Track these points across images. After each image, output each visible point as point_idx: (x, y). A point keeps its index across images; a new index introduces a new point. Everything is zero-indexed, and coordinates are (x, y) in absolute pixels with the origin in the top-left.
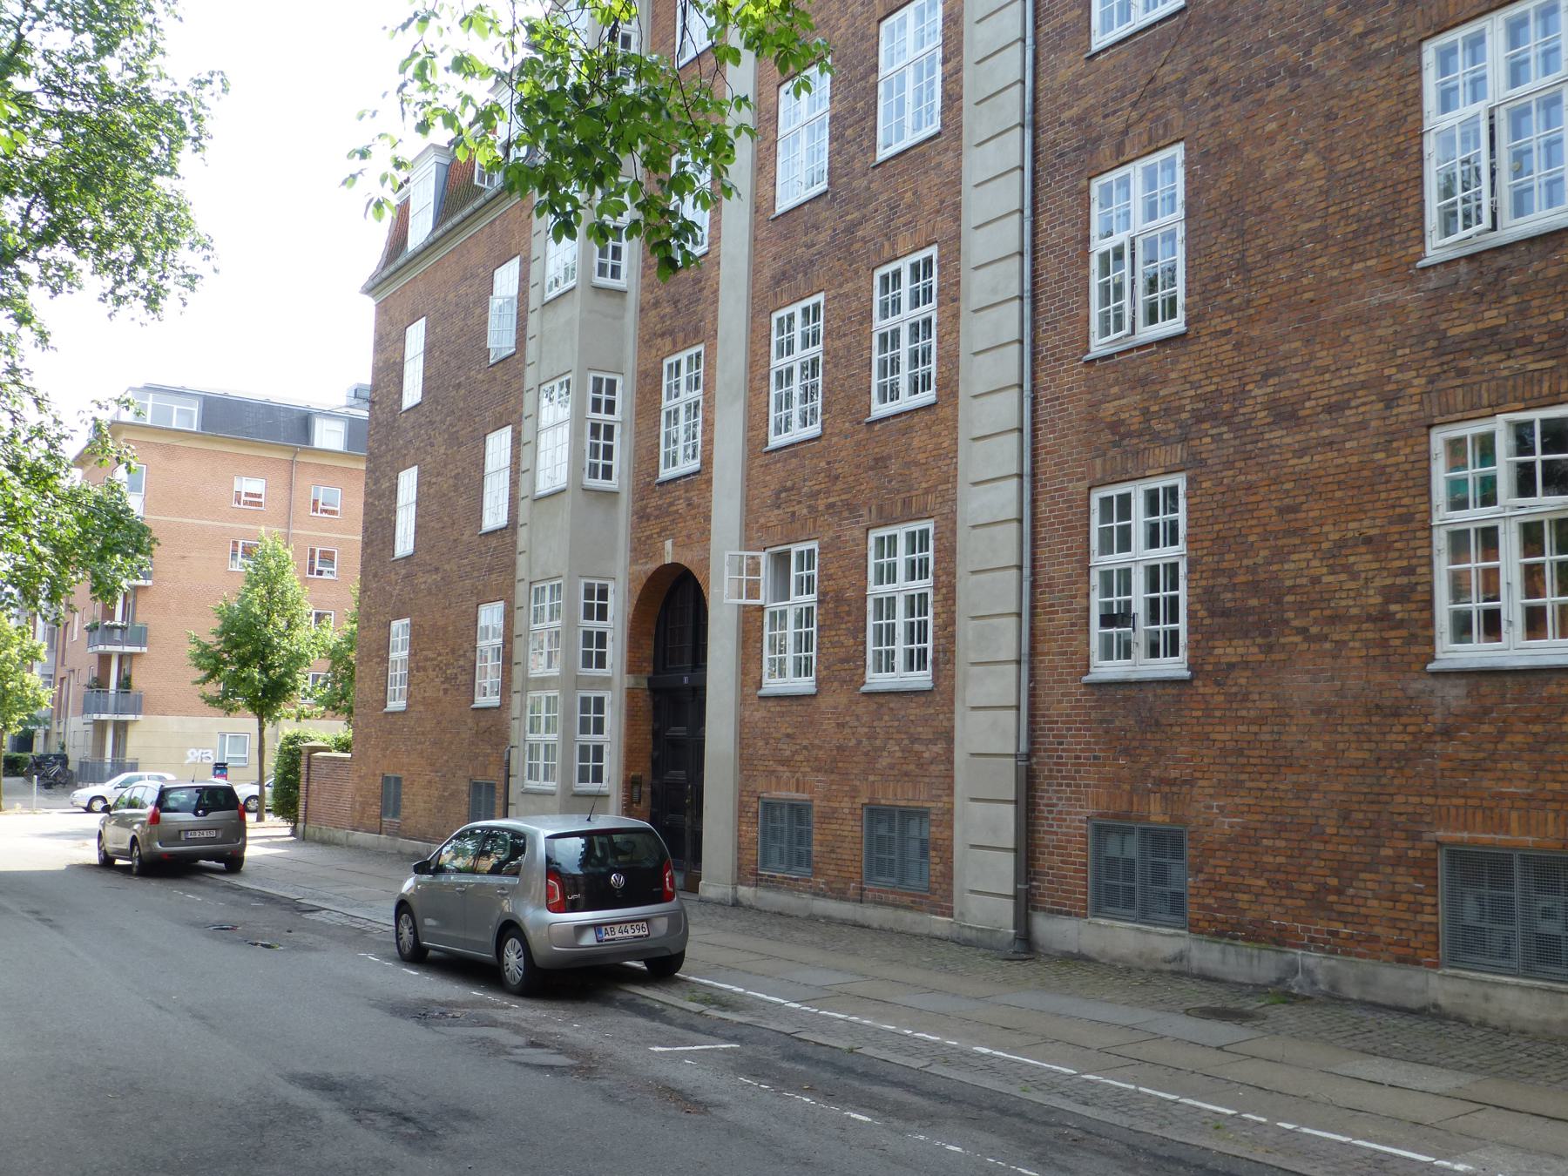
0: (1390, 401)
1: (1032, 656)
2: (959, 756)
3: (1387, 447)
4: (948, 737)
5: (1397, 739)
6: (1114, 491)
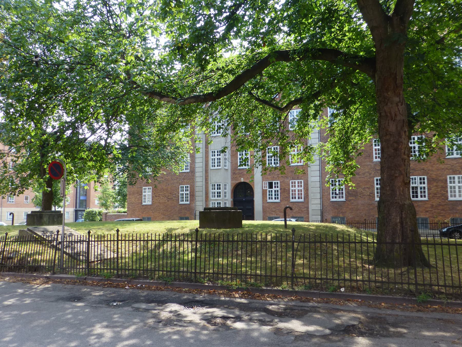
0: (370, 174)
1: (322, 198)
2: (310, 210)
3: (370, 178)
4: (308, 208)
5: (371, 207)
6: (182, 186)
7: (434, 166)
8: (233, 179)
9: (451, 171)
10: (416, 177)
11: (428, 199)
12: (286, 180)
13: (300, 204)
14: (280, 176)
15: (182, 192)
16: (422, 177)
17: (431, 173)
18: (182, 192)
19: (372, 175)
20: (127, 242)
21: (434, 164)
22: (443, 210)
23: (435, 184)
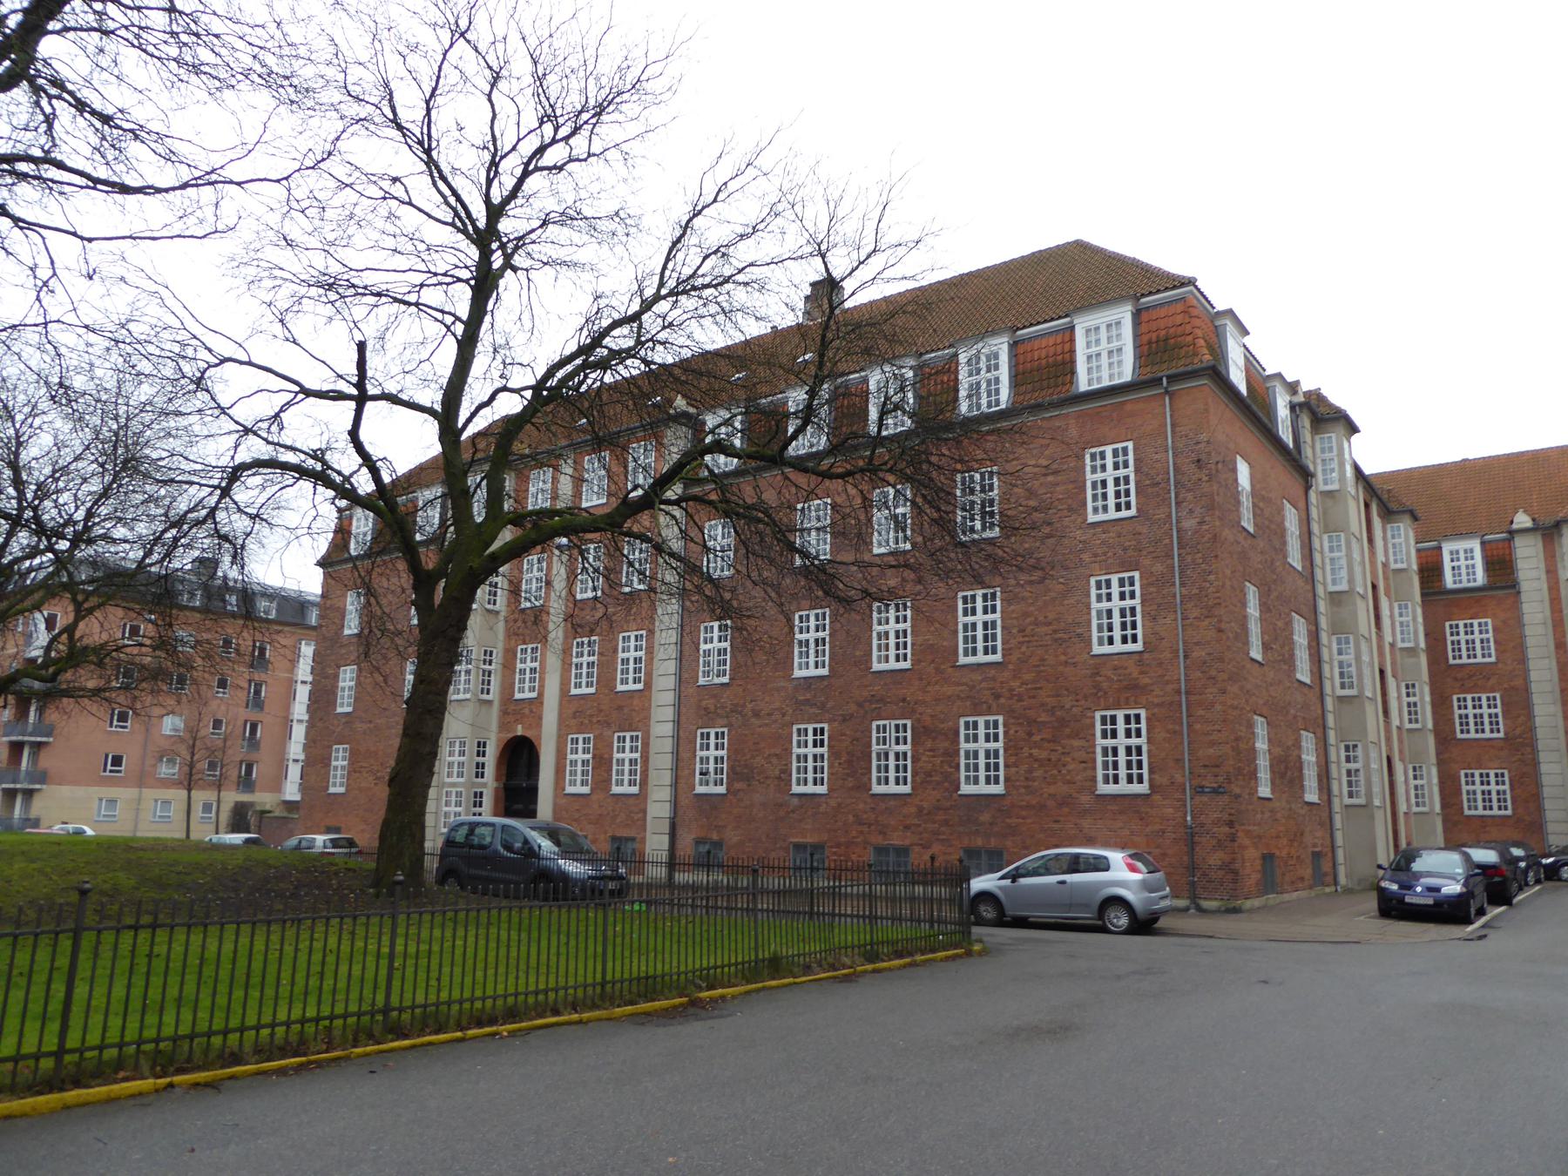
1: (675, 784)
5: (782, 813)
6: (802, 726)
7: (929, 688)
8: (503, 726)
9: (968, 703)
10: (887, 722)
11: (913, 788)
12: (607, 733)
13: (631, 801)
14: (595, 720)
15: (971, 746)
16: (1132, 712)
17: (920, 709)
18: (971, 746)
19: (787, 718)
20: (849, 944)
21: (929, 683)
22: (946, 823)
23: (929, 744)
